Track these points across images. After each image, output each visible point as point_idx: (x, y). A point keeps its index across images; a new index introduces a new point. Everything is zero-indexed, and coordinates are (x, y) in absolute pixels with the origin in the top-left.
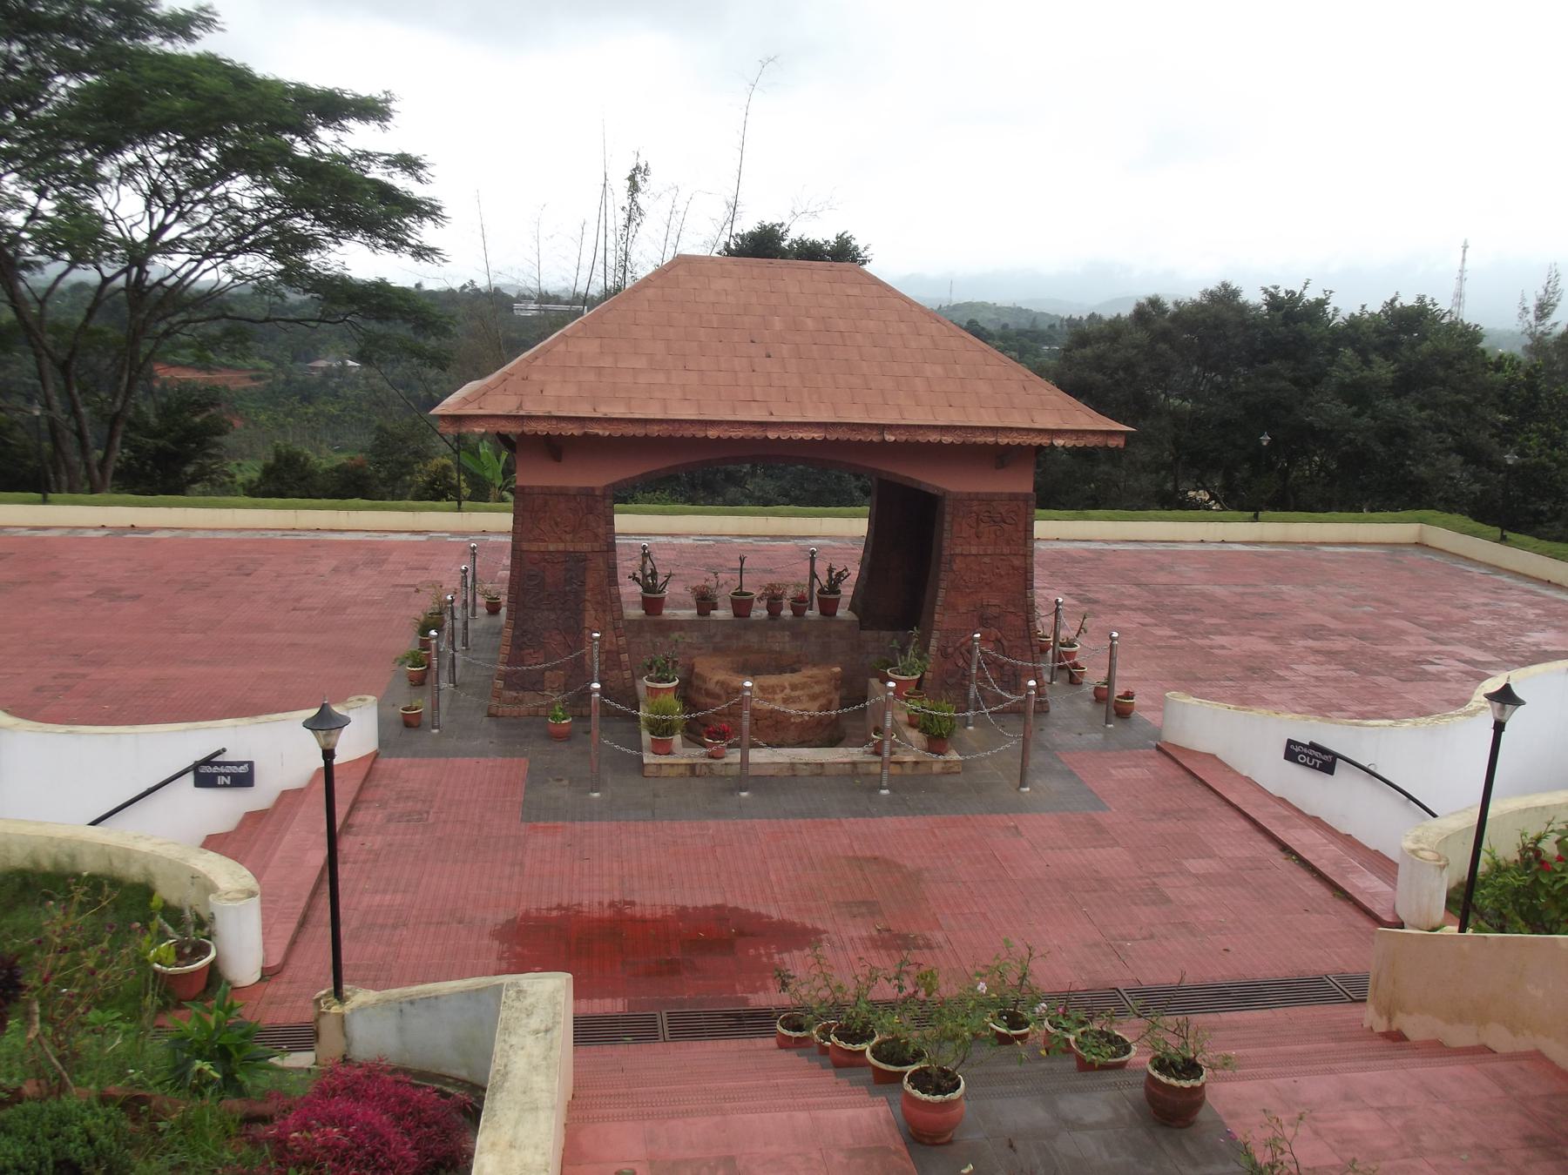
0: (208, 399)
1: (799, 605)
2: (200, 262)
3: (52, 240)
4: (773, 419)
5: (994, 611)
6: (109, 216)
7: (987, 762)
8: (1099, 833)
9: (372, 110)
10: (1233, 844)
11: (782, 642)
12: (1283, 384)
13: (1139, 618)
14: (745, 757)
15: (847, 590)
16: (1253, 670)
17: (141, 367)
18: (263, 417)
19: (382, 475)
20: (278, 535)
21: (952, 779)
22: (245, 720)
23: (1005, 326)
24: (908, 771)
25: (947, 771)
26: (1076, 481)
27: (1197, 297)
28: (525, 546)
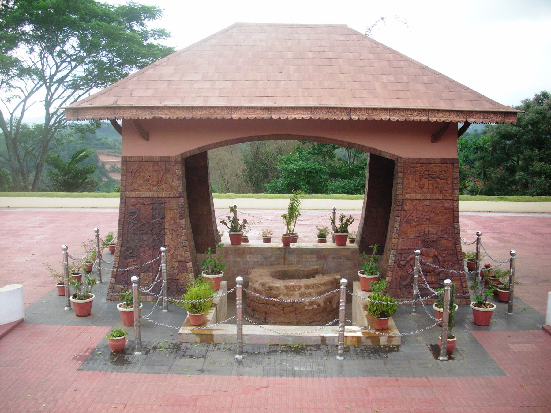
14: (240, 329)
15: (354, 229)
28: (128, 194)
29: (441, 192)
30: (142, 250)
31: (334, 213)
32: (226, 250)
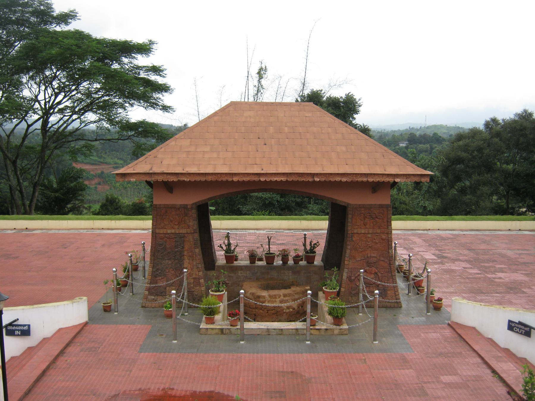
1: (297, 259)
2: (71, 116)
4: (262, 172)
5: (374, 260)
8: (404, 362)
9: (144, 49)
11: (289, 276)
13: (464, 265)
15: (320, 250)
16: (511, 289)
17: (46, 162)
20: (85, 231)
22: (28, 307)
24: (323, 333)
25: (342, 333)
27: (512, 117)
28: (157, 231)
29: (379, 228)
30: (167, 271)
31: (305, 238)
32: (222, 267)
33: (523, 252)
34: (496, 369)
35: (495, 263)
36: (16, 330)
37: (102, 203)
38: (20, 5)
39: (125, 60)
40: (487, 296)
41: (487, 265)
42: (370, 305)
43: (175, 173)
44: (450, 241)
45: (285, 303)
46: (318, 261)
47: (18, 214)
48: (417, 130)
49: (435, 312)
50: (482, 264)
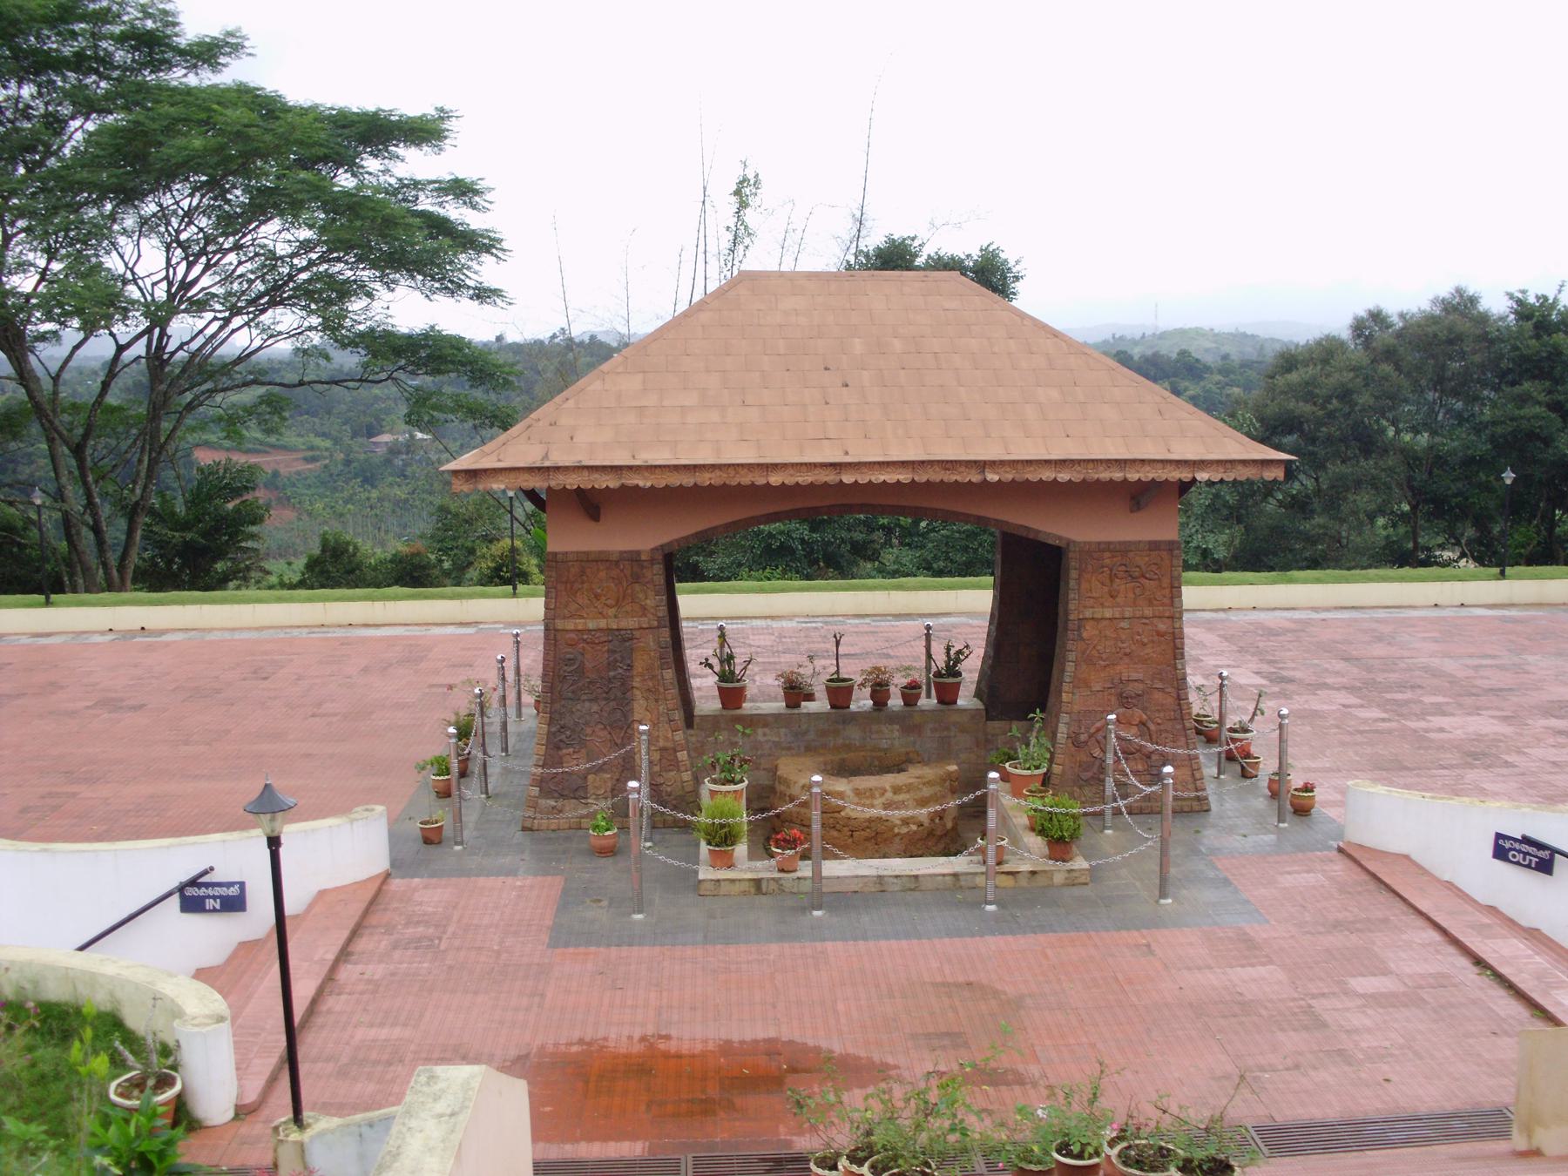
0: (239, 483)
1: (910, 693)
2: (227, 321)
3: (60, 305)
6: (129, 276)
7: (1124, 872)
8: (1249, 949)
9: (424, 132)
10: (1415, 956)
11: (891, 738)
12: (1537, 409)
13: (1343, 698)
15: (971, 669)
16: (1475, 756)
17: (162, 447)
18: (319, 505)
19: (446, 565)
21: (1076, 891)
22: (236, 835)
23: (1225, 357)
24: (1023, 882)
25: (1072, 881)
26: (1268, 532)
27: (1426, 306)
28: (560, 624)
29: (1150, 604)
33: (1484, 662)
34: (1484, 956)
35: (1419, 692)
36: (209, 897)
37: (310, 557)
38: (83, 18)
39: (371, 164)
40: (1418, 776)
41: (1399, 696)
42: (1146, 809)
43: (612, 467)
44: (1290, 637)
45: (897, 808)
46: (966, 699)
47: (87, 591)
48: (1135, 343)
49: (1296, 819)
50: (1389, 696)
